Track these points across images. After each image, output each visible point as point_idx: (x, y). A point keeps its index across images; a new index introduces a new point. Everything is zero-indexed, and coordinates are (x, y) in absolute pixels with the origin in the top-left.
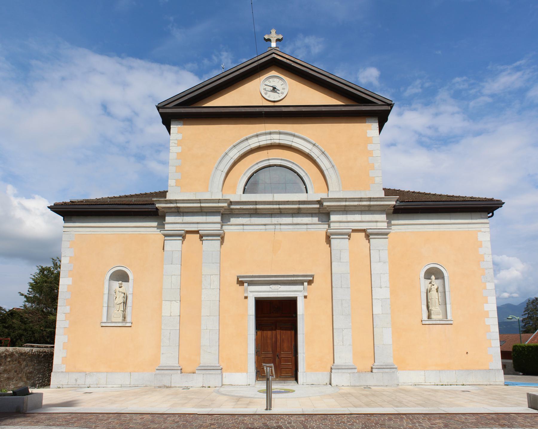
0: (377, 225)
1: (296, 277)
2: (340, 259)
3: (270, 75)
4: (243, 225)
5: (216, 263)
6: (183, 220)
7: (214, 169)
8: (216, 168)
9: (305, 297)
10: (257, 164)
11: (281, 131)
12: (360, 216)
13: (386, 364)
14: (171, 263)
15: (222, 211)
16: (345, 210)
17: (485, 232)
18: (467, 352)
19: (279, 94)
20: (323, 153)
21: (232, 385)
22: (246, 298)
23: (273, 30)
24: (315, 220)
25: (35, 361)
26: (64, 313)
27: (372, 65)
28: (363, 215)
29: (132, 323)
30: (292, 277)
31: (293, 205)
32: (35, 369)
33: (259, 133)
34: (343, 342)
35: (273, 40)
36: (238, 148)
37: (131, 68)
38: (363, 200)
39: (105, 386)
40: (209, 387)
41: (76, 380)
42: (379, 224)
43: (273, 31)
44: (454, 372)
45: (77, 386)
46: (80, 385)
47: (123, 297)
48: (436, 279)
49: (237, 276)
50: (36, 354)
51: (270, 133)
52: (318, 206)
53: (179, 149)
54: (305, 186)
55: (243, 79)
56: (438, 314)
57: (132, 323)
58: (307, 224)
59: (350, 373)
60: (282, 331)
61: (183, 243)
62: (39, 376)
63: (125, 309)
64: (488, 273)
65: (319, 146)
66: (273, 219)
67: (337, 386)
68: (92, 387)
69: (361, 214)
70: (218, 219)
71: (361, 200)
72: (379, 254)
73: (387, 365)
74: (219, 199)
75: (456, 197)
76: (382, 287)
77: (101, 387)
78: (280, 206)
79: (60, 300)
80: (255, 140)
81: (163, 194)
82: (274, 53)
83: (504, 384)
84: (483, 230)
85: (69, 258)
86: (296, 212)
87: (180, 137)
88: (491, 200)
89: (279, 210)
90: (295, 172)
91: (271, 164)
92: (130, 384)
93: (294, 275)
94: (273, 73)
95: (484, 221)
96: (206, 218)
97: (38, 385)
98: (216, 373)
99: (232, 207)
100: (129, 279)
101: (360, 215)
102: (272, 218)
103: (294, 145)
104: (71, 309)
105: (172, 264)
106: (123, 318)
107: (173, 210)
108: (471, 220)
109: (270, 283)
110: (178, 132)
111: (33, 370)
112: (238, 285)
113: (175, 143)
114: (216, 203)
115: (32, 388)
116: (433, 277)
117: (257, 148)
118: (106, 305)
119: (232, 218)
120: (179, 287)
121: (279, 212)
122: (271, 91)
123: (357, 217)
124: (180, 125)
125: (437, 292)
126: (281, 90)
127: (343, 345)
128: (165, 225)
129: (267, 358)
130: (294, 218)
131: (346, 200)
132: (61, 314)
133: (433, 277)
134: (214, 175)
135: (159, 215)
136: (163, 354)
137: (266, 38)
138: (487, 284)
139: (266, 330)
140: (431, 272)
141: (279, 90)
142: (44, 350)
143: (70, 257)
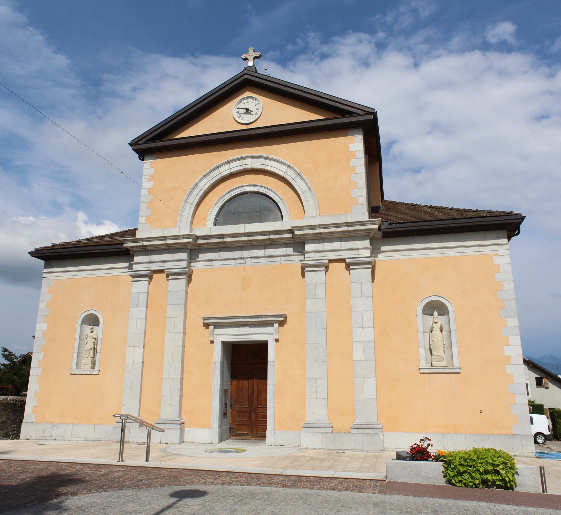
0: (358, 253)
1: (264, 317)
2: (315, 295)
3: (244, 97)
4: (212, 260)
5: (181, 304)
6: (150, 259)
7: (183, 202)
8: (186, 201)
9: (277, 340)
10: (229, 192)
11: (254, 154)
12: (339, 243)
13: (368, 423)
14: (137, 305)
15: (189, 247)
16: (322, 238)
17: (503, 256)
18: (481, 411)
19: (253, 115)
20: (299, 174)
21: (193, 442)
22: (212, 342)
23: (251, 49)
24: (290, 250)
25: (9, 410)
26: (38, 360)
27: (505, 19)
28: (342, 242)
29: (99, 371)
30: (261, 318)
31: (263, 236)
32: (9, 419)
33: (229, 159)
34: (316, 395)
35: (251, 58)
36: (209, 177)
37: (205, 67)
38: (339, 225)
39: (70, 439)
40: (167, 444)
41: (44, 432)
42: (360, 252)
43: (251, 50)
44: (464, 436)
45: (44, 438)
46: (47, 437)
47: (94, 342)
48: (439, 315)
49: (205, 319)
50: (11, 402)
51: (242, 158)
52: (290, 235)
53: (150, 185)
54: (280, 213)
55: (215, 105)
56: (441, 360)
57: (99, 371)
58: (280, 256)
59: (322, 433)
60: (260, 381)
61: (149, 283)
62: (14, 426)
63: (95, 355)
64: (509, 305)
65: (295, 167)
66: (243, 252)
67: (307, 448)
68: (58, 440)
69: (341, 242)
70: (184, 255)
71: (337, 225)
72: (361, 287)
73: (369, 424)
74: (184, 235)
75: (474, 211)
76: (364, 327)
77: (66, 440)
78: (249, 237)
79: (36, 346)
80: (226, 167)
81: (133, 232)
82: (246, 74)
83: (535, 456)
84: (500, 253)
85: (46, 302)
86: (269, 243)
87: (152, 171)
88: (509, 214)
89: (250, 243)
90: (270, 198)
91: (243, 191)
92: (93, 438)
93: (262, 315)
94: (248, 94)
95: (502, 242)
96: (173, 256)
97: (11, 436)
98: (175, 428)
99: (200, 242)
100: (99, 324)
101: (338, 243)
102: (243, 251)
103: (268, 168)
104: (44, 356)
105: (137, 307)
106: (91, 365)
107: (141, 248)
108: (483, 241)
109: (239, 325)
110: (150, 166)
111: (7, 420)
112: (205, 328)
113: (147, 179)
114: (181, 239)
115: (5, 439)
116: (436, 313)
117: (228, 175)
118: (76, 351)
119: (201, 253)
120: (143, 332)
121: (250, 244)
122: (245, 113)
123: (336, 245)
124: (152, 160)
125: (441, 331)
126: (254, 111)
127: (317, 398)
128: (132, 265)
129: (242, 412)
130: (266, 250)
131: (320, 227)
132: (35, 361)
133: (436, 313)
134: (182, 210)
135: (131, 255)
136: (124, 405)
137: (243, 58)
138: (508, 320)
139: (242, 380)
140: (435, 306)
141: (252, 112)
142: (21, 399)
143: (48, 302)
